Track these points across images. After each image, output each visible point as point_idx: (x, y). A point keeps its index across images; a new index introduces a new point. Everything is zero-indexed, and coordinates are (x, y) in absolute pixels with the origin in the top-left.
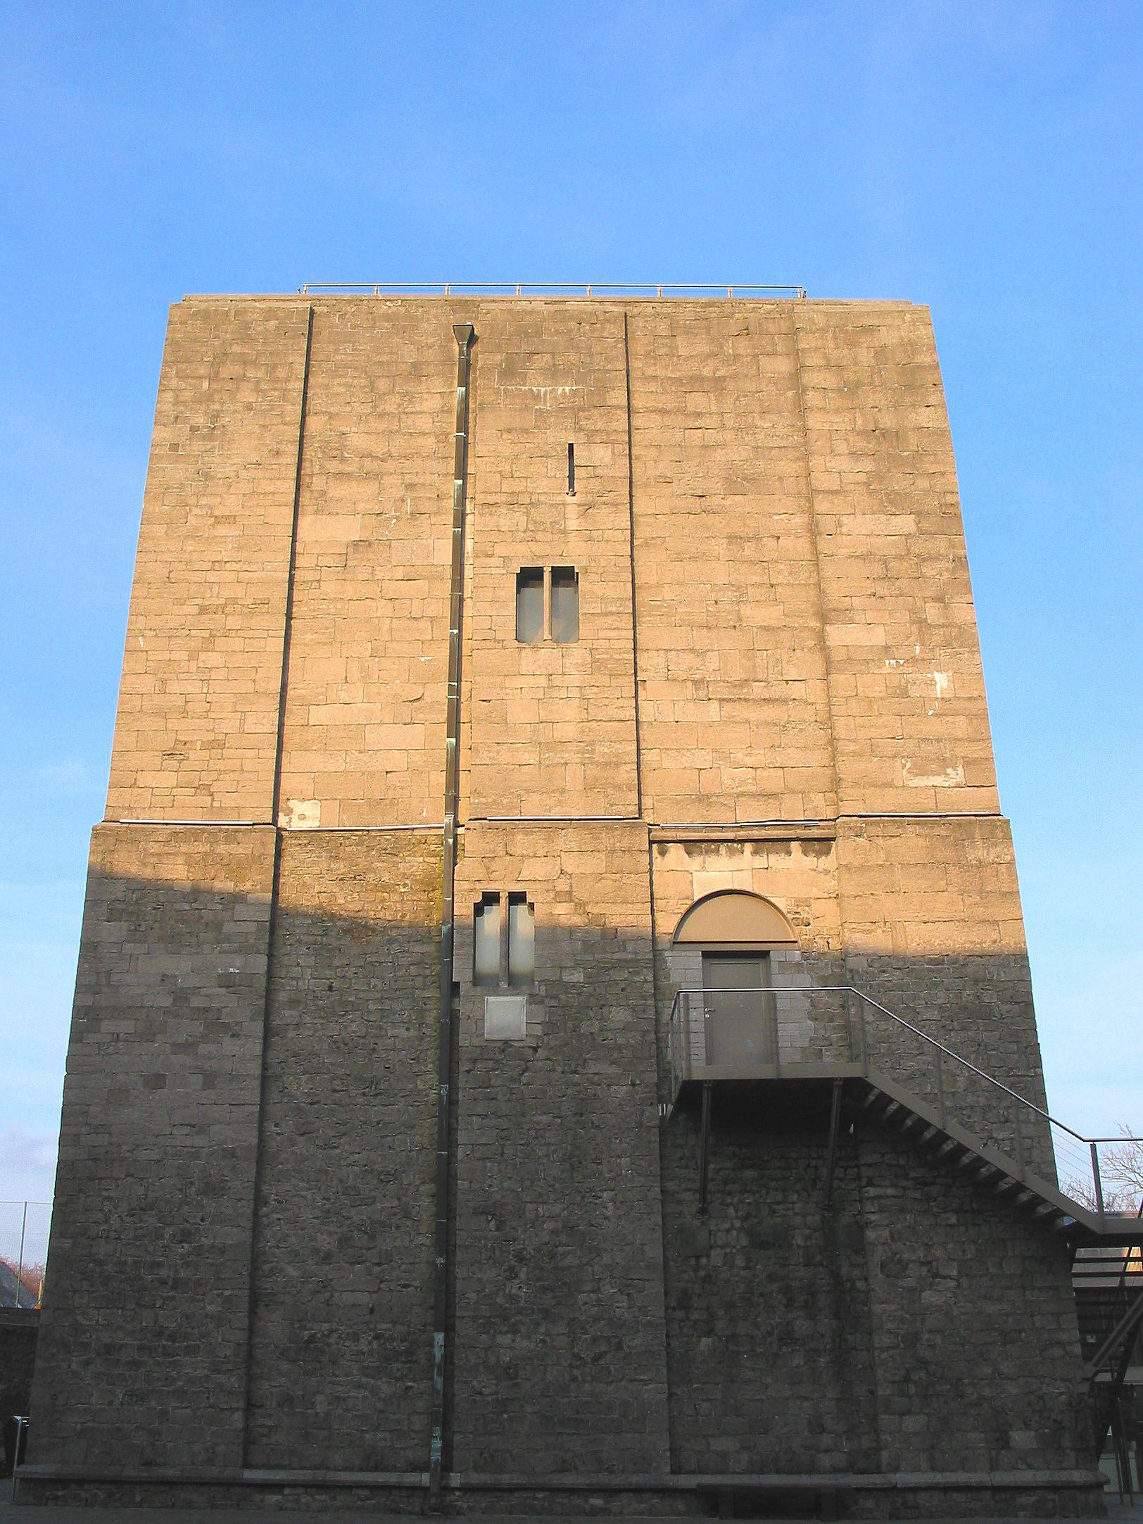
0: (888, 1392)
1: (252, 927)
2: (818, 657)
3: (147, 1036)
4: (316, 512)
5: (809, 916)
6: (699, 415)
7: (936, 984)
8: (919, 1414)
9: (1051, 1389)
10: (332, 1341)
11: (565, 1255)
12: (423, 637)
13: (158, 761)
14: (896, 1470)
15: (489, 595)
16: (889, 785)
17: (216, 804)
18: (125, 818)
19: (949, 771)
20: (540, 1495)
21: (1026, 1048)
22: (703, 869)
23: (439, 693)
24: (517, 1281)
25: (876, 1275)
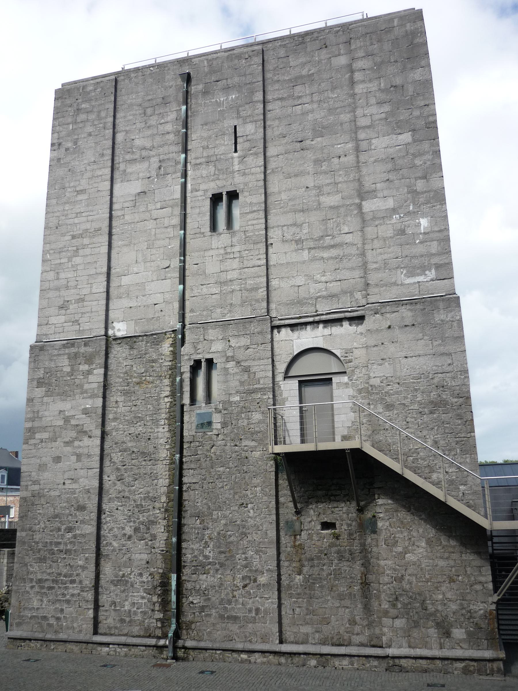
0: (387, 606)
1: (95, 385)
2: (359, 219)
3: (54, 439)
4: (122, 181)
5: (352, 358)
6: (300, 97)
7: (416, 390)
8: (403, 618)
9: (475, 607)
10: (132, 577)
11: (230, 536)
12: (170, 236)
13: (57, 311)
14: (390, 647)
15: (197, 211)
16: (395, 284)
17: (81, 329)
18: (45, 339)
19: (427, 272)
20: (218, 652)
21: (466, 422)
22: (299, 338)
23: (176, 263)
24: (209, 549)
25: (382, 545)
